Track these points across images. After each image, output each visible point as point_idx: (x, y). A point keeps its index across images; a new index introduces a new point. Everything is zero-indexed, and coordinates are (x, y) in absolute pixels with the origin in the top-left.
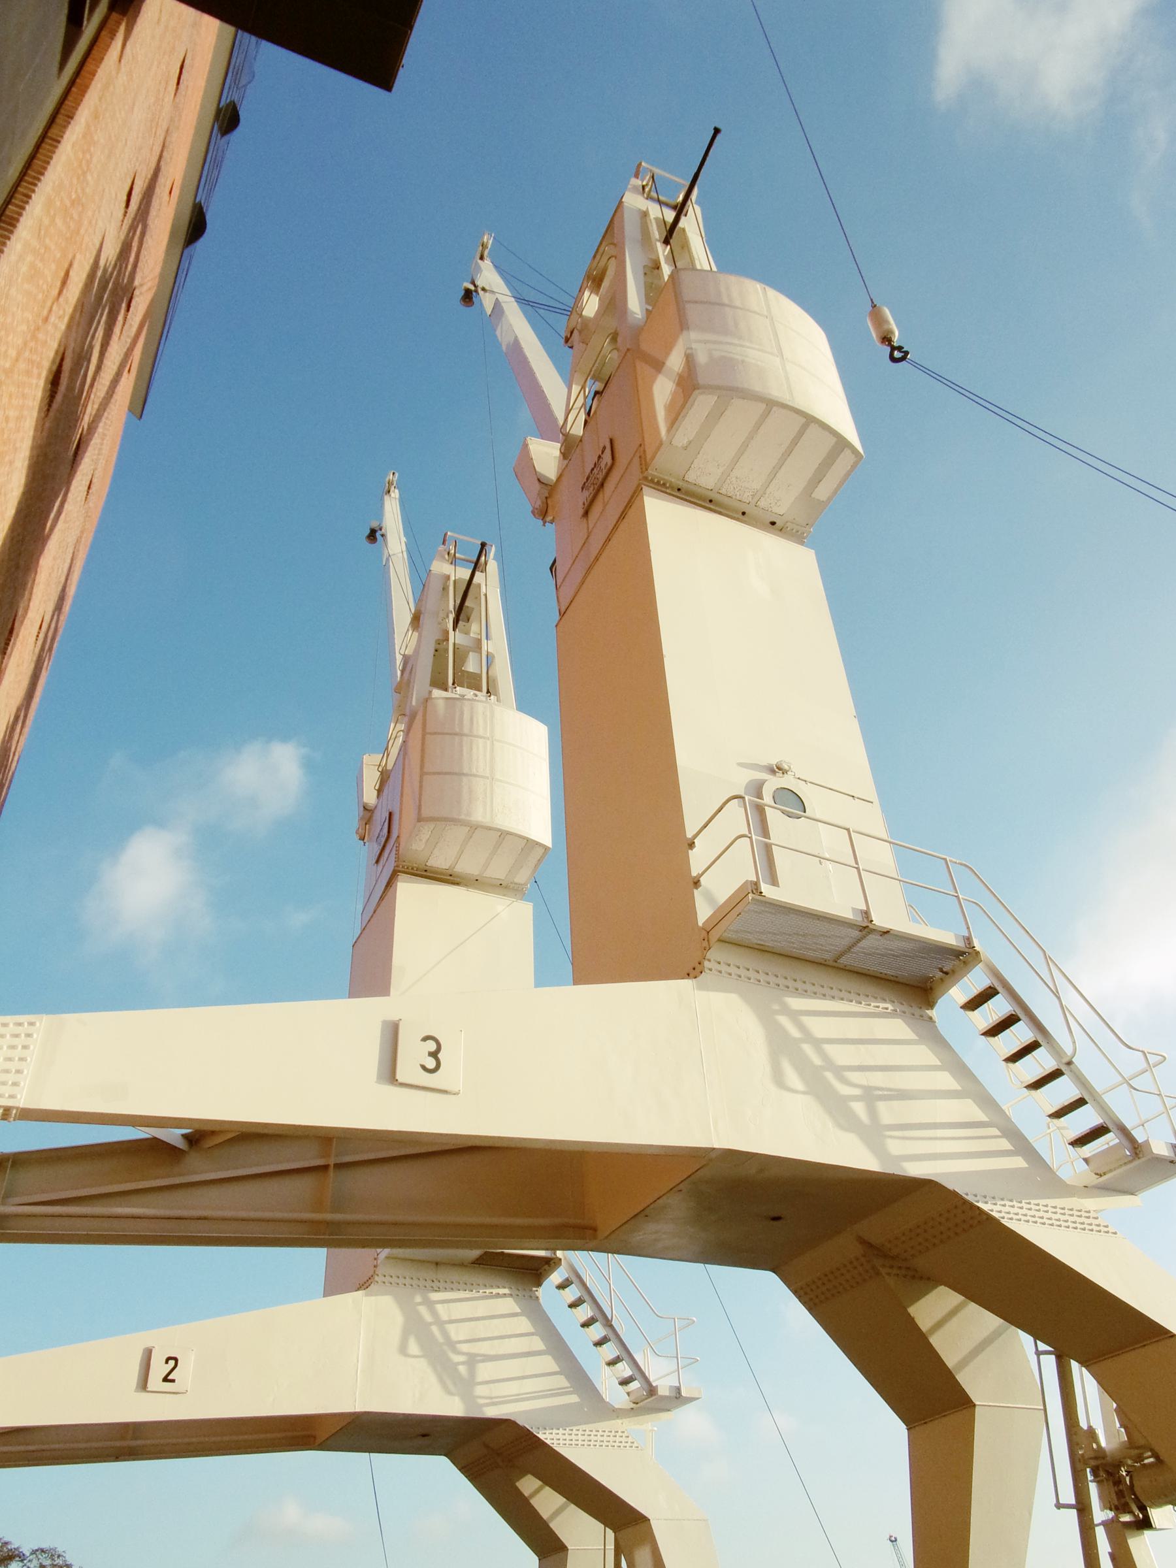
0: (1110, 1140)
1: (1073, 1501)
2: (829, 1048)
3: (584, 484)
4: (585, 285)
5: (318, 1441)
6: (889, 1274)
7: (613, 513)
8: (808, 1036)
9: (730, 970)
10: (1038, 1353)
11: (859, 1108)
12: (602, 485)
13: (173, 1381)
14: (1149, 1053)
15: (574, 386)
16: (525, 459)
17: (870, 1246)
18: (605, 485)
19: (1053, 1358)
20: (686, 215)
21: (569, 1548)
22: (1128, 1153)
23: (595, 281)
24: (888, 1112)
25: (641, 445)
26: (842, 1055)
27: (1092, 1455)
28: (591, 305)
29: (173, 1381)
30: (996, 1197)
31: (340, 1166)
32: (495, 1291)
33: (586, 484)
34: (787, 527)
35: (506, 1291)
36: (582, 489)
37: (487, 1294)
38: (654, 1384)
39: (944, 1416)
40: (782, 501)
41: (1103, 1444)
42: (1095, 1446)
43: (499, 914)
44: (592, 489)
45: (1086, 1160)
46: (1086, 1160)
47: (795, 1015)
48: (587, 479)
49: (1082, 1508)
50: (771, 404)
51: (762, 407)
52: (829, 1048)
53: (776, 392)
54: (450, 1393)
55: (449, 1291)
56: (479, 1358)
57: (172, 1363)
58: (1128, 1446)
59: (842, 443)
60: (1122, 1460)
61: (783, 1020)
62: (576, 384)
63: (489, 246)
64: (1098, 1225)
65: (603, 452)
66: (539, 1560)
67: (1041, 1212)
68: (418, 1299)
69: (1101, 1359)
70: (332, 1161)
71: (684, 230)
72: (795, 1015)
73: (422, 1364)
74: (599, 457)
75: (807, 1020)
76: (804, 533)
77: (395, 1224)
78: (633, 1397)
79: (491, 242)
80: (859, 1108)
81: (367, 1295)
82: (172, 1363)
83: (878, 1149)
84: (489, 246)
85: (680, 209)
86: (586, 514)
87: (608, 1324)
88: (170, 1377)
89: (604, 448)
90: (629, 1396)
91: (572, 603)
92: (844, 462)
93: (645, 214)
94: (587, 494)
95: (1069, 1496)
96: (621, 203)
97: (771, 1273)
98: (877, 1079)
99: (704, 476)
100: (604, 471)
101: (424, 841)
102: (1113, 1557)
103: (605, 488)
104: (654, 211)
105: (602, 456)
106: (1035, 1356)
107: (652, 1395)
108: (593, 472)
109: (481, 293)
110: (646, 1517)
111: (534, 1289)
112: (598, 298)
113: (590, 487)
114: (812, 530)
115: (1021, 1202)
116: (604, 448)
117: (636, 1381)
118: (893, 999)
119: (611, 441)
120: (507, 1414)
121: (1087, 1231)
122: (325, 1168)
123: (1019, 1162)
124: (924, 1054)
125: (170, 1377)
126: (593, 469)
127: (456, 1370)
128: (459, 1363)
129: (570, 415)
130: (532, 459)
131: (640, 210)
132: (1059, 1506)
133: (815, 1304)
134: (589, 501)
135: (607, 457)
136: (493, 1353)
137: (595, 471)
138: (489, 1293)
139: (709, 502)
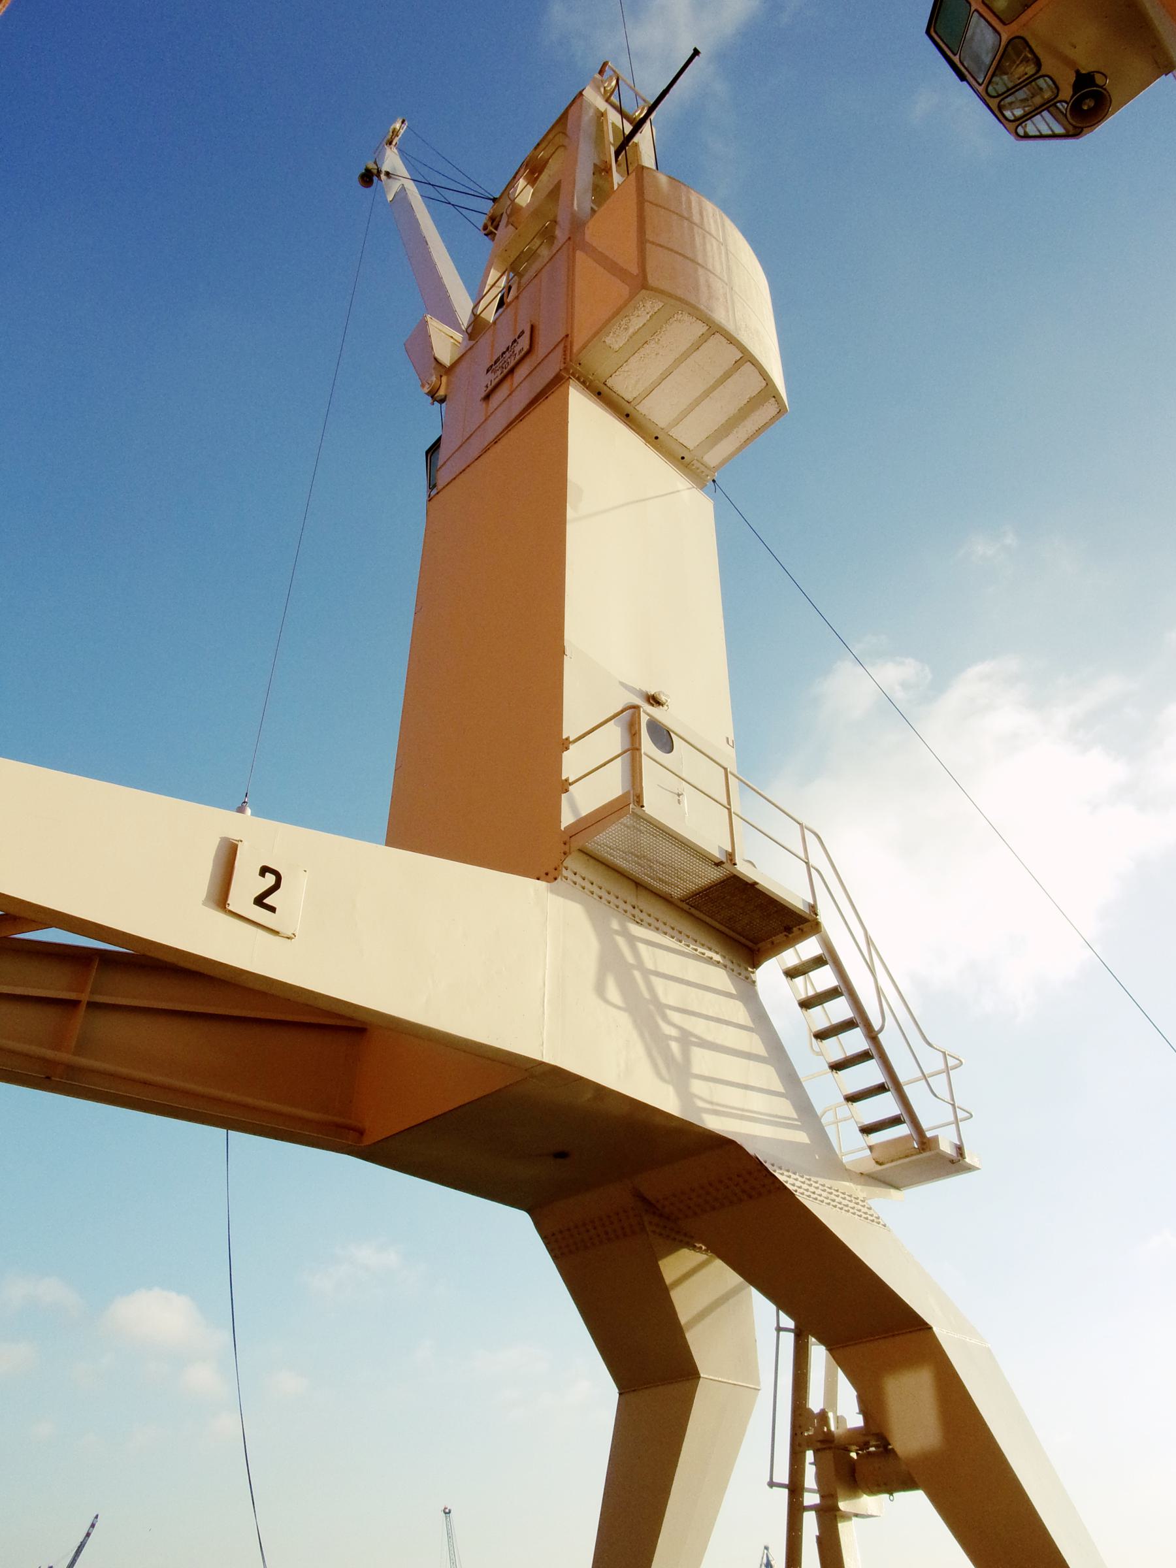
0: (903, 1130)
1: (786, 1481)
2: (658, 982)
3: (491, 366)
4: (521, 173)
5: (368, 1141)
6: (654, 1232)
7: (521, 399)
8: (640, 965)
9: (576, 878)
10: (779, 1329)
11: (675, 1046)
12: (512, 371)
13: (272, 909)
14: (948, 1055)
15: (492, 270)
16: (422, 336)
17: (643, 1199)
18: (491, 397)
19: (791, 1336)
20: (641, 133)
21: (702, 1375)
22: (916, 1146)
23: (533, 169)
24: (702, 1060)
25: (567, 336)
26: (668, 994)
27: (821, 1438)
28: (524, 194)
29: (272, 909)
30: (783, 1168)
31: (93, 1005)
32: (709, 954)
33: (494, 367)
34: (693, 465)
35: (717, 958)
36: (488, 371)
37: (697, 953)
38: (929, 1134)
39: (646, 1388)
40: (689, 435)
41: (833, 1428)
42: (825, 1429)
43: (678, 491)
44: (499, 372)
45: (871, 1148)
46: (871, 1148)
47: (632, 940)
48: (496, 363)
49: (795, 1488)
50: (715, 329)
51: (700, 329)
52: (658, 982)
53: (720, 316)
54: (662, 1079)
55: (652, 930)
56: (694, 1039)
57: (270, 879)
58: (864, 1432)
59: (768, 391)
60: (847, 1446)
61: (621, 941)
62: (494, 269)
63: (400, 136)
64: (872, 1215)
65: (519, 337)
66: (620, 1394)
67: (819, 1190)
68: (615, 925)
69: (904, 1331)
70: (85, 997)
71: (636, 145)
72: (632, 940)
73: (624, 1019)
74: (515, 341)
75: (641, 947)
76: (708, 476)
77: (145, 1083)
78: (876, 1154)
79: (402, 131)
80: (675, 1046)
81: (552, 891)
82: (270, 879)
83: (685, 1094)
84: (400, 136)
85: (638, 126)
86: (487, 398)
87: (872, 1036)
88: (267, 901)
89: (523, 332)
90: (871, 1151)
91: (479, 459)
92: (770, 409)
93: (602, 115)
94: (494, 378)
95: (783, 1476)
96: (581, 94)
97: (526, 1213)
98: (699, 1027)
99: (625, 385)
100: (518, 357)
101: (631, 331)
102: (820, 1540)
103: (515, 374)
104: (614, 117)
105: (519, 340)
106: (776, 1333)
107: (924, 1150)
108: (504, 356)
109: (383, 176)
110: (927, 1324)
111: (750, 969)
112: (532, 190)
113: (498, 370)
114: (716, 474)
115: (802, 1177)
116: (523, 332)
117: (905, 1124)
118: (717, 950)
119: (532, 328)
120: (723, 1131)
121: (856, 1216)
122: (74, 1004)
123: (802, 1137)
124: (738, 1012)
125: (267, 901)
126: (504, 353)
127: (668, 1047)
128: (670, 1038)
129: (482, 301)
130: (430, 336)
131: (598, 109)
132: (772, 1484)
133: (562, 1254)
134: (493, 384)
135: (524, 343)
136: (709, 1038)
137: (507, 354)
138: (700, 953)
139: (627, 415)
